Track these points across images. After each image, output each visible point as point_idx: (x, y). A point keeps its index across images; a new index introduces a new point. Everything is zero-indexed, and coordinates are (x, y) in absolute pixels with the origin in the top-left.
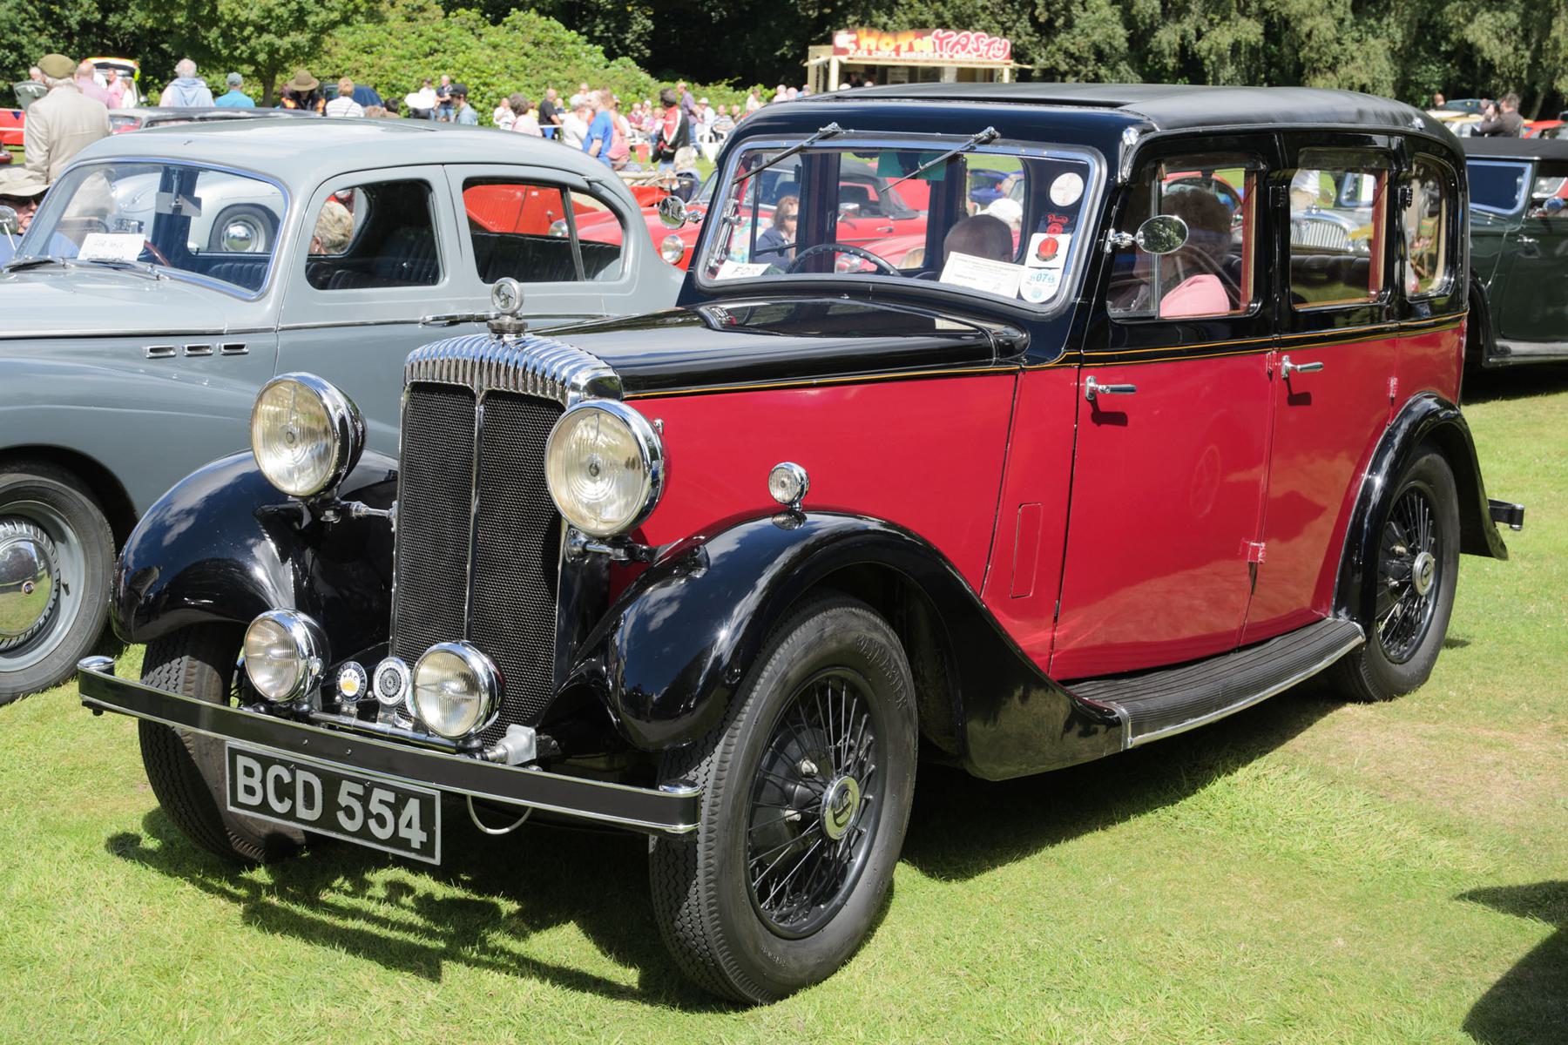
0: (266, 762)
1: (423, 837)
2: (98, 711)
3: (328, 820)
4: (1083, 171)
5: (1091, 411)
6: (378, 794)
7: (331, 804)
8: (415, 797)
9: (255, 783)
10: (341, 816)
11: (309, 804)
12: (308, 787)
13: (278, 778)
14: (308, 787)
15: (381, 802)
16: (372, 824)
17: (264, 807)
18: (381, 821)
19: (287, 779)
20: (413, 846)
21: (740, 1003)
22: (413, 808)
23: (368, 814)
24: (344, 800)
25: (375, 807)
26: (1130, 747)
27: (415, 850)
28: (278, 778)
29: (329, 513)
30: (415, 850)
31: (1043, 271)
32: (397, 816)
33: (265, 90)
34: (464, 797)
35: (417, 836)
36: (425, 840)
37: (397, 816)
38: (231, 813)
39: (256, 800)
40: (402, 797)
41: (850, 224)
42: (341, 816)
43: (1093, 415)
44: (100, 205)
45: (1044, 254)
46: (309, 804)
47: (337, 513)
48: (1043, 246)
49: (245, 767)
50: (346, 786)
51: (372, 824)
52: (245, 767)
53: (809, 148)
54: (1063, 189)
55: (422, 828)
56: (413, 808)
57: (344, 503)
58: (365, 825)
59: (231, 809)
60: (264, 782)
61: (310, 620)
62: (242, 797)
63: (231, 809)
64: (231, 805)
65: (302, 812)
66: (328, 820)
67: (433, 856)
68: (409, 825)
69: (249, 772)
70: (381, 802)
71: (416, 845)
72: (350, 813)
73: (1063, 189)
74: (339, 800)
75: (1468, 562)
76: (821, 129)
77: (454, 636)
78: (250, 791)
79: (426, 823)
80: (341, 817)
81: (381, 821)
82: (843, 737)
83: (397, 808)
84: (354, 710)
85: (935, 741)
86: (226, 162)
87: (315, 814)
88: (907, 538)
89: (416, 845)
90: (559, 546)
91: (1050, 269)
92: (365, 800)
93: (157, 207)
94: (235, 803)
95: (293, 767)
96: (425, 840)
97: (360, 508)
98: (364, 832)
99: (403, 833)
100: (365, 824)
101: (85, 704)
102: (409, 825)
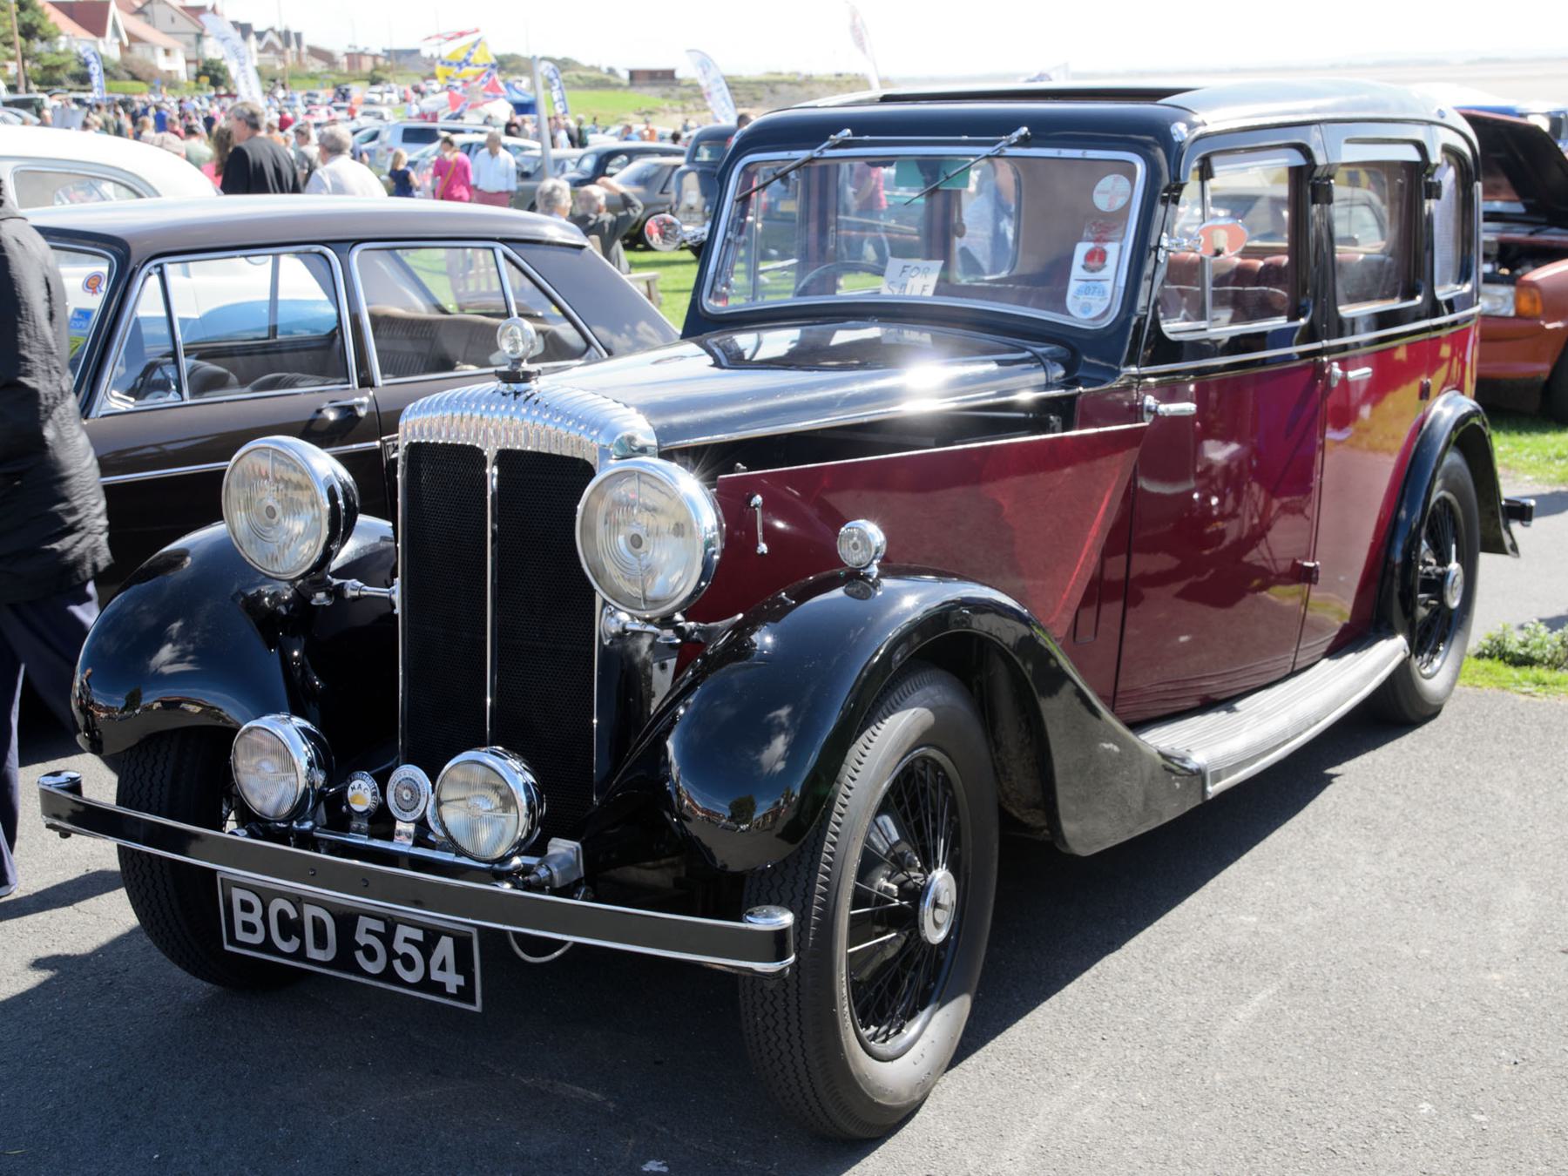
0: (266, 896)
1: (460, 980)
2: (65, 834)
3: (345, 959)
4: (1130, 172)
6: (403, 932)
8: (448, 935)
9: (255, 918)
10: (359, 955)
11: (321, 942)
12: (319, 925)
13: (282, 915)
14: (319, 925)
15: (407, 940)
16: (397, 964)
17: (267, 946)
18: (409, 963)
19: (293, 914)
20: (448, 990)
22: (446, 947)
23: (392, 955)
24: (362, 938)
25: (400, 947)
26: (1210, 797)
27: (451, 996)
28: (282, 915)
29: (321, 596)
30: (451, 996)
31: (1090, 284)
32: (427, 957)
34: (505, 932)
35: (453, 981)
36: (462, 983)
37: (427, 957)
38: (228, 952)
39: (257, 939)
40: (432, 936)
42: (359, 955)
45: (1091, 264)
46: (321, 942)
47: (329, 595)
48: (1090, 256)
49: (241, 900)
50: (364, 923)
51: (397, 964)
52: (241, 900)
53: (817, 158)
54: (1107, 192)
55: (458, 971)
56: (446, 947)
57: (336, 582)
58: (389, 966)
60: (265, 919)
61: (307, 724)
62: (241, 935)
63: (228, 948)
65: (313, 953)
66: (345, 959)
67: (473, 1002)
68: (443, 967)
69: (247, 907)
70: (407, 940)
71: (451, 989)
72: (370, 953)
73: (1107, 192)
74: (357, 938)
75: (1486, 560)
76: (832, 137)
77: (478, 742)
78: (249, 928)
79: (463, 965)
81: (409, 963)
83: (427, 948)
84: (365, 825)
85: (1016, 814)
86: (208, 433)
87: (328, 955)
89: (451, 989)
90: (594, 627)
91: (1099, 281)
92: (387, 938)
94: (233, 940)
95: (298, 901)
96: (462, 983)
97: (353, 587)
98: (389, 975)
99: (436, 975)
100: (389, 966)
101: (49, 826)
102: (443, 967)
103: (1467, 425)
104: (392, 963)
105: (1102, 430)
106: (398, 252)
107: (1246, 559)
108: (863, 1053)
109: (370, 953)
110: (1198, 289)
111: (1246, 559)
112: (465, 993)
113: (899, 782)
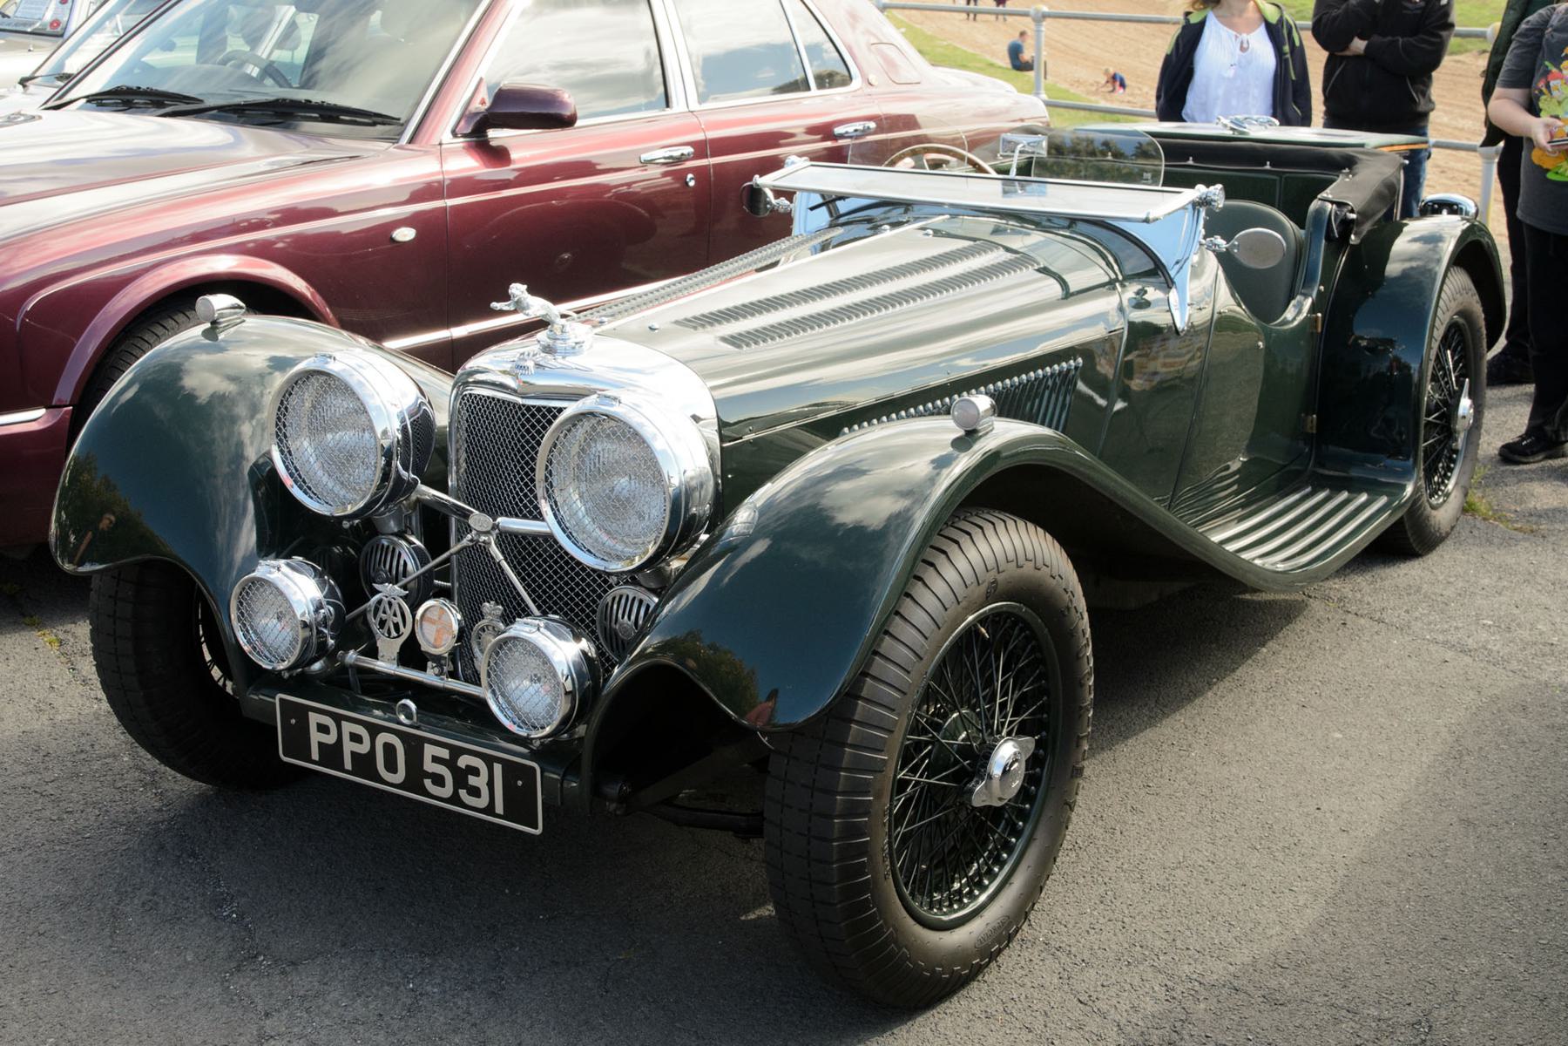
3: (416, 776)
10: (428, 783)
11: (391, 766)
20: (497, 811)
24: (429, 766)
42: (428, 783)
46: (391, 766)
49: (350, 733)
52: (350, 733)
66: (416, 776)
67: (281, 700)
87: (399, 777)
103: (688, 554)
104: (458, 793)
105: (505, 564)
106: (56, 90)
107: (1126, 404)
108: (905, 914)
109: (439, 780)
110: (449, 584)
111: (1126, 404)
113: (971, 633)
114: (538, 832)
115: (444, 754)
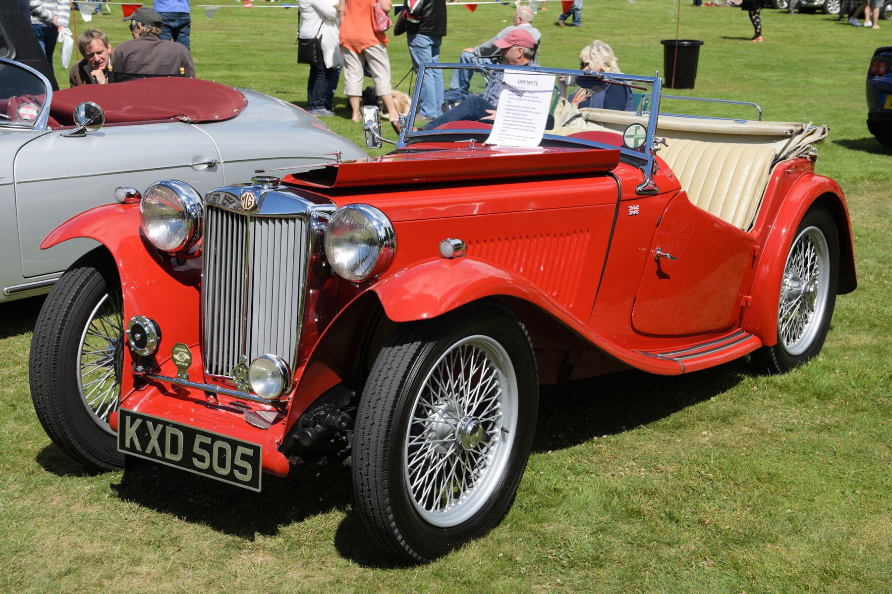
3: (188, 459)
5: (657, 269)
7: (189, 453)
11: (174, 451)
12: (174, 438)
14: (174, 438)
21: (404, 562)
24: (197, 449)
33: (324, 258)
41: (548, 8)
43: (657, 271)
44: (581, 20)
46: (174, 451)
50: (199, 439)
51: (237, 473)
59: (119, 450)
63: (119, 450)
64: (120, 448)
65: (168, 455)
66: (188, 459)
80: (196, 462)
82: (440, 385)
87: (178, 457)
88: (443, 209)
93: (756, 120)
98: (231, 476)
112: (253, 482)
114: (259, 490)
115: (208, 441)
